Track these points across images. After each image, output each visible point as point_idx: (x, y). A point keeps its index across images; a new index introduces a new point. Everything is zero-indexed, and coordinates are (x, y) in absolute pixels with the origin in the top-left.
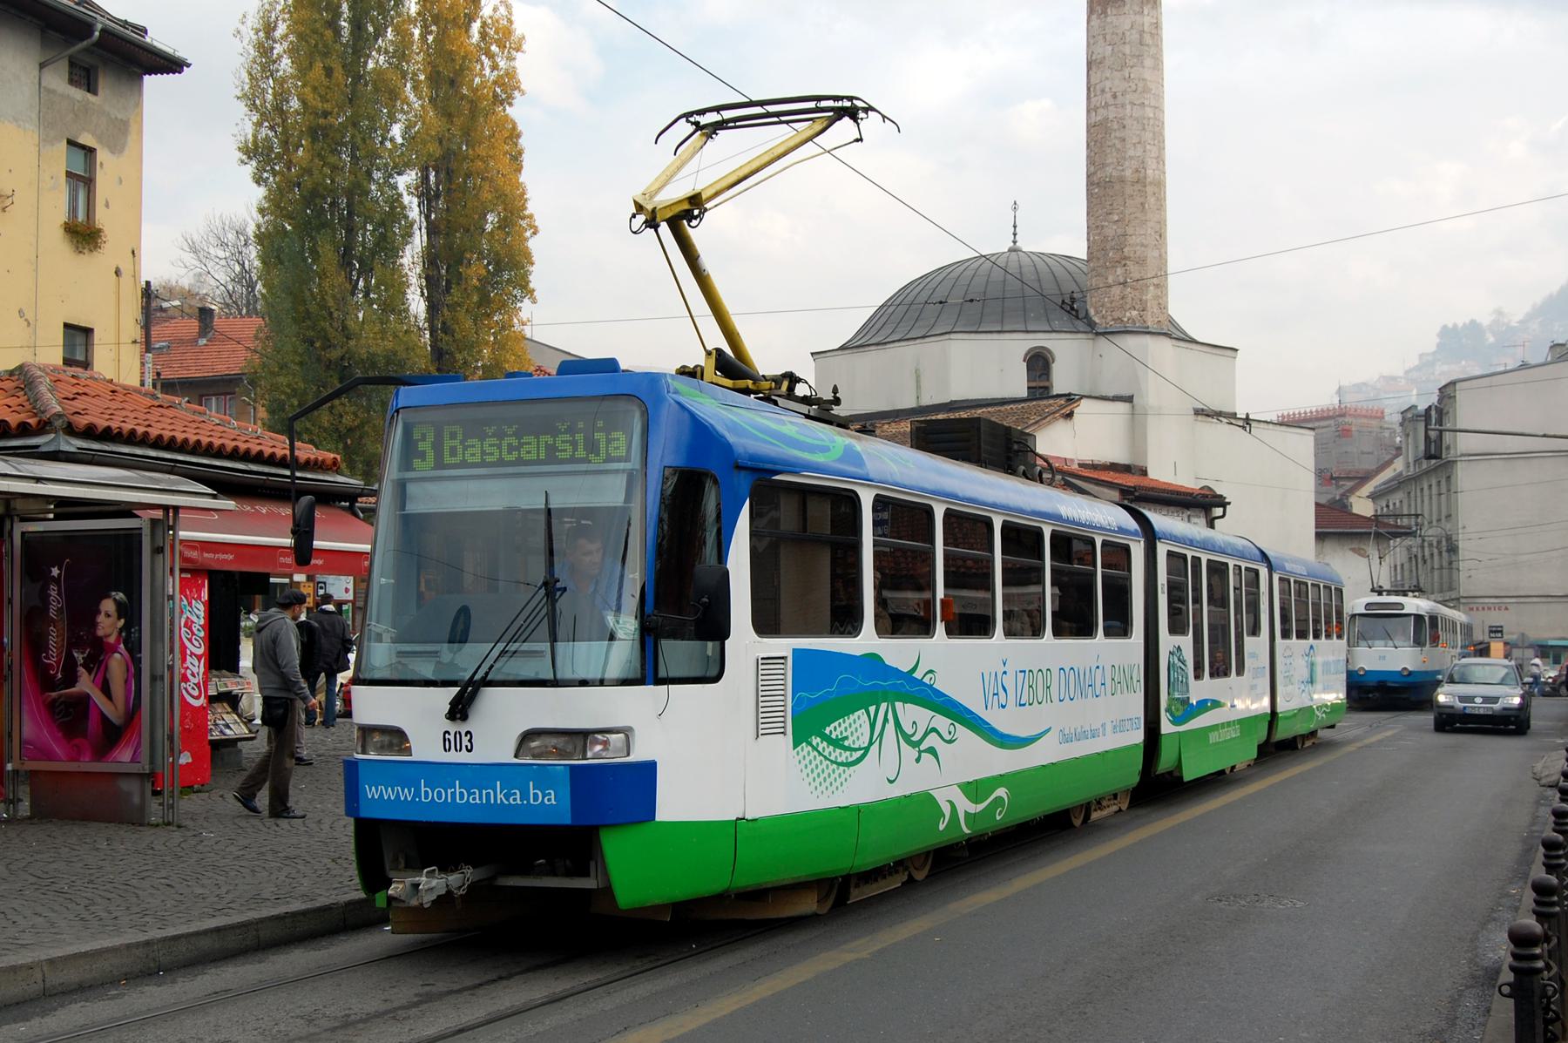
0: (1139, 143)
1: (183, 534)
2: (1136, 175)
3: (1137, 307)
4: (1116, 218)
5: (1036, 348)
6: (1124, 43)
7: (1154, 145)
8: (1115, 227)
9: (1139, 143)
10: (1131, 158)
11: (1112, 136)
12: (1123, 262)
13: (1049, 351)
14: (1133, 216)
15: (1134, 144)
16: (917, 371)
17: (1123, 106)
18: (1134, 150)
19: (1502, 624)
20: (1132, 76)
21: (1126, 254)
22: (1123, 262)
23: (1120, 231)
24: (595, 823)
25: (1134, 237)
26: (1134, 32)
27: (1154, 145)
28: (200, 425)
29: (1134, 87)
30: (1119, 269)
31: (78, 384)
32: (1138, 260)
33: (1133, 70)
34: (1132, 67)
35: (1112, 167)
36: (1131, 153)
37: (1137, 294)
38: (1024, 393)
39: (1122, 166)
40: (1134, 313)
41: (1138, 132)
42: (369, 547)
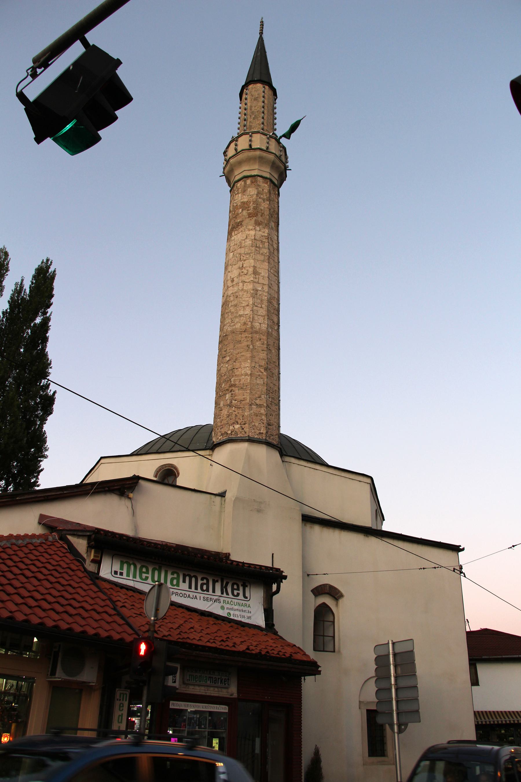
0: (247, 306)
1: (186, 735)
2: (244, 327)
3: (239, 422)
4: (228, 358)
5: (165, 465)
6: (241, 247)
7: (261, 307)
8: (227, 366)
9: (247, 306)
10: (241, 316)
11: (230, 306)
12: (230, 389)
13: (176, 468)
14: (240, 355)
15: (244, 307)
16: (262, 22)
17: (237, 284)
18: (244, 311)
19: (11, 290)
20: (244, 266)
21: (233, 383)
22: (230, 389)
23: (230, 367)
24: (473, 712)
25: (240, 370)
26: (248, 240)
27: (261, 307)
28: (241, 632)
29: (245, 272)
30: (227, 395)
31: (133, 608)
32: (242, 386)
33: (245, 262)
34: (244, 260)
35: (228, 325)
36: (241, 312)
37: (240, 411)
38: (467, 631)
39: (234, 322)
40: (237, 426)
41: (247, 299)
42: (34, 650)
